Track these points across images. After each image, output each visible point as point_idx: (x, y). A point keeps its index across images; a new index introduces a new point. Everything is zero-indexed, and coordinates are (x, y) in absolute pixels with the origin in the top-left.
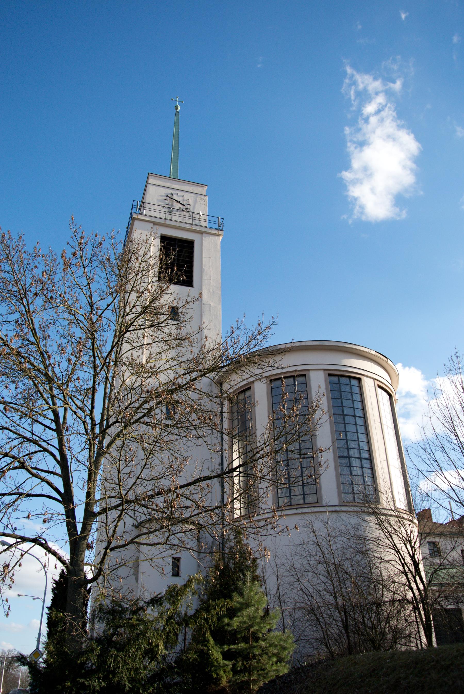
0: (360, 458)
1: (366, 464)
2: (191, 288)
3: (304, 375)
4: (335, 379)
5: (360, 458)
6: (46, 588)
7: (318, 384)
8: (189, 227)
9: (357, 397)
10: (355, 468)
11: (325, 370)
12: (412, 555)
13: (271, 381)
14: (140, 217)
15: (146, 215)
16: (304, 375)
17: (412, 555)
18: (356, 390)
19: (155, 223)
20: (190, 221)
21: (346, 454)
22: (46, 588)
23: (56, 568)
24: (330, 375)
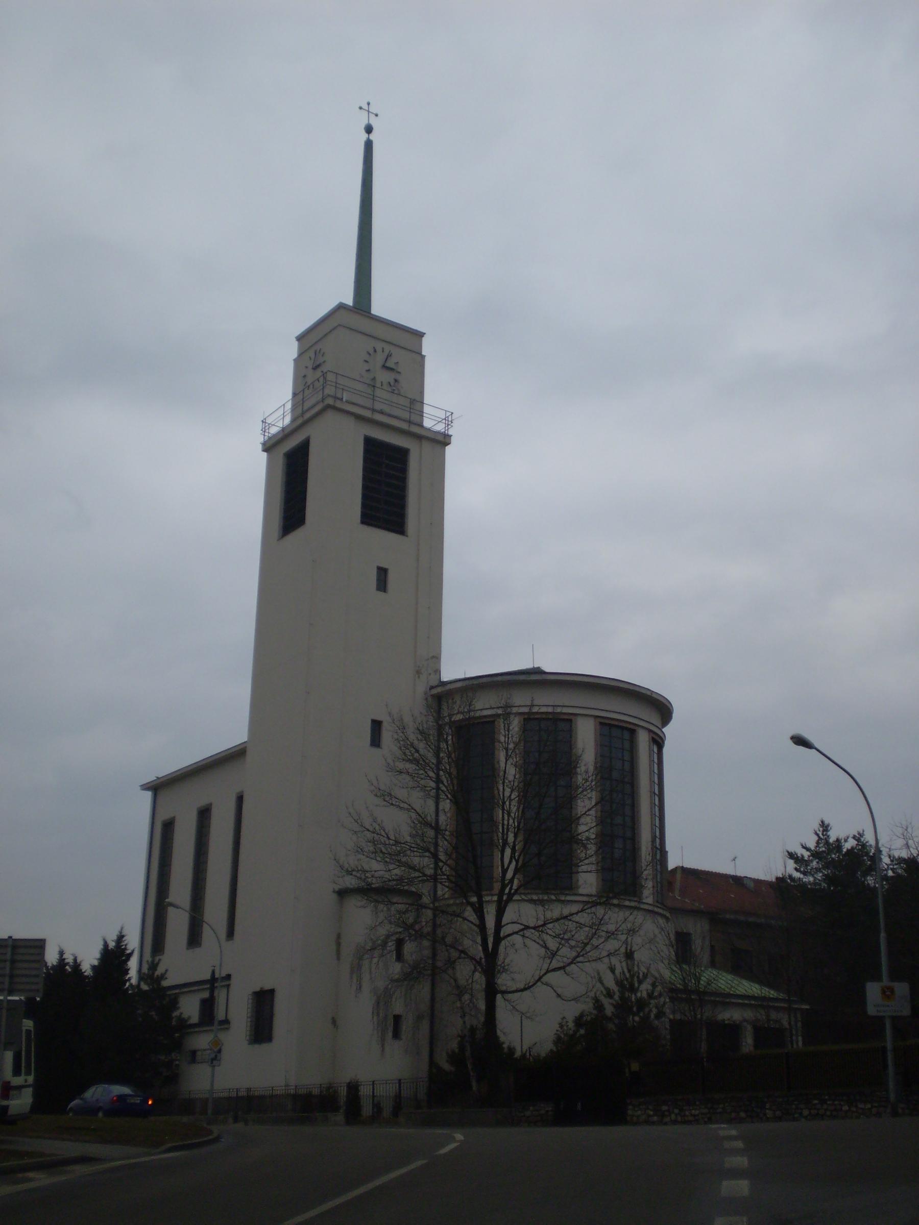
8: (404, 426)
14: (339, 404)
18: (627, 745)
19: (359, 418)
24: (601, 723)
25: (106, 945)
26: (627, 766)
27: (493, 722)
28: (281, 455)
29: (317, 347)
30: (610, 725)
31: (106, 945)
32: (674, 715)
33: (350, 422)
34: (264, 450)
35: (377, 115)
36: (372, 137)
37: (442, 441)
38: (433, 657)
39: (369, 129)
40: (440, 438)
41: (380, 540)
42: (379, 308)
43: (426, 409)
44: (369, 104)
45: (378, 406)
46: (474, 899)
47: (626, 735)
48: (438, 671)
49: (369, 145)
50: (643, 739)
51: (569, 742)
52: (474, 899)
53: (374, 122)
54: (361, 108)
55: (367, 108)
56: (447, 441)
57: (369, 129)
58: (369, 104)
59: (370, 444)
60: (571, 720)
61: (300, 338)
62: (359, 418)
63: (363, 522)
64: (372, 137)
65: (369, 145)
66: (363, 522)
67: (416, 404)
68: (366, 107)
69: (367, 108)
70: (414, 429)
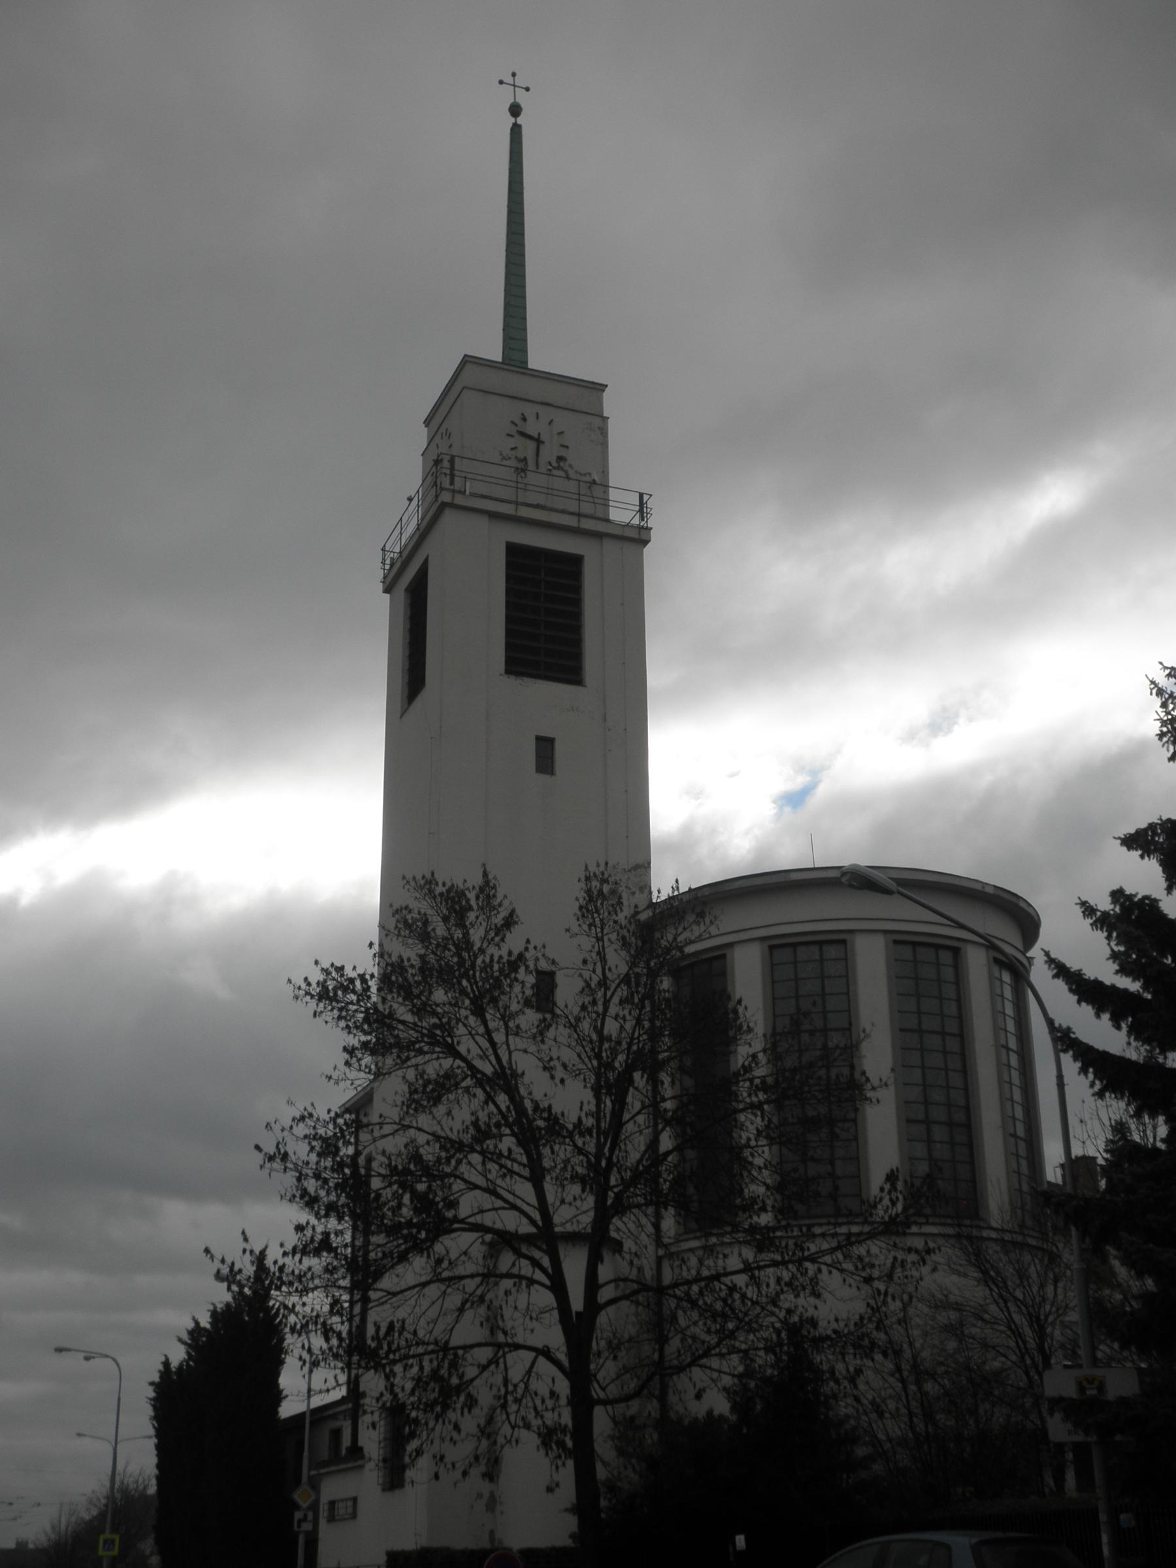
0: (943, 1034)
1: (953, 1045)
2: (579, 688)
3: (843, 942)
4: (907, 953)
5: (943, 1034)
6: (119, 1399)
7: (871, 965)
8: (571, 521)
9: (949, 991)
10: (938, 1146)
11: (886, 932)
12: (577, 1303)
13: (771, 948)
14: (459, 500)
15: (472, 495)
16: (843, 942)
17: (577, 1303)
18: (948, 973)
19: (493, 516)
20: (572, 506)
21: (921, 1116)
22: (119, 1399)
23: (59, 1350)
24: (896, 942)
25: (166, 1364)
26: (951, 1009)
27: (724, 956)
28: (403, 592)
29: (442, 430)
30: (914, 944)
31: (166, 1364)
32: (1042, 930)
33: (483, 522)
34: (386, 591)
35: (527, 89)
36: (520, 120)
37: (638, 538)
38: (637, 867)
39: (515, 110)
40: (633, 534)
41: (542, 698)
42: (537, 360)
43: (613, 494)
44: (514, 75)
45: (533, 498)
46: (929, 1386)
47: (946, 957)
48: (646, 888)
49: (516, 131)
50: (976, 961)
51: (847, 977)
52: (929, 1386)
53: (522, 98)
54: (501, 82)
55: (511, 81)
56: (644, 537)
57: (515, 110)
58: (514, 75)
59: (513, 550)
60: (844, 942)
61: (427, 422)
62: (493, 516)
63: (508, 672)
64: (520, 120)
65: (516, 131)
66: (508, 672)
67: (596, 487)
68: (510, 80)
69: (511, 81)
70: (600, 527)
